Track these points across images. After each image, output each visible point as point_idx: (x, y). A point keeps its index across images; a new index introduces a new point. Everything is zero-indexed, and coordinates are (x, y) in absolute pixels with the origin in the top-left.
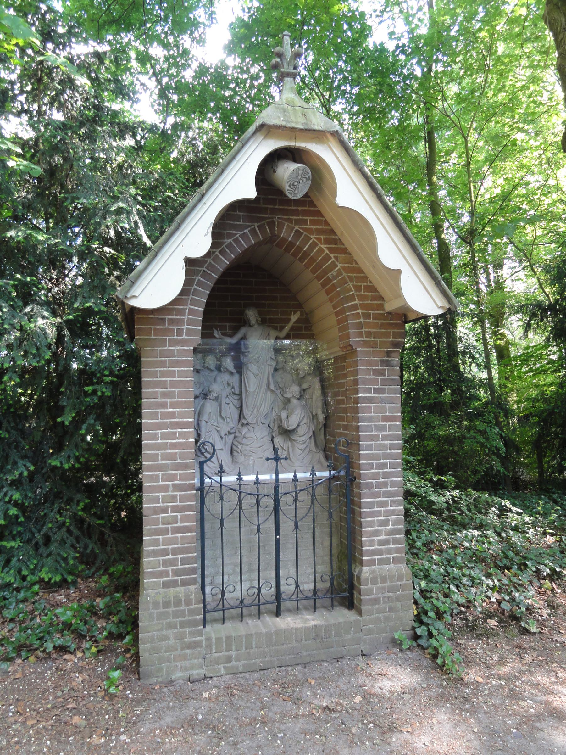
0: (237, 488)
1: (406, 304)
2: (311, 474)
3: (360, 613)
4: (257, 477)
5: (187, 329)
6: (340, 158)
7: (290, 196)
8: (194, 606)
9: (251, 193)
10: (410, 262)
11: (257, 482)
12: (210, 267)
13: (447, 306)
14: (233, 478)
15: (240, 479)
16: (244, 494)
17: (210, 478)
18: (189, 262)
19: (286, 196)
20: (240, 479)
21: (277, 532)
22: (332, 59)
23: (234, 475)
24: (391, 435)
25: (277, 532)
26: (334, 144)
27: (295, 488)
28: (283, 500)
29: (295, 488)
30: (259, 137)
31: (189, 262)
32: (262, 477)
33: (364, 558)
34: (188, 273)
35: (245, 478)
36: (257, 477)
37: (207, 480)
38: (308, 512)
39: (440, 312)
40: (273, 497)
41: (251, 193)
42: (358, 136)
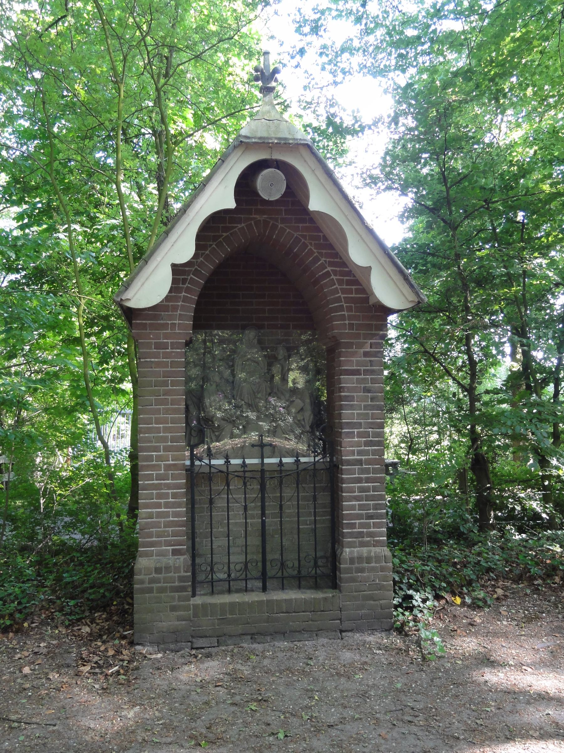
0: (224, 469)
1: (379, 302)
3: (340, 591)
4: (281, 460)
6: (398, 284)
8: (183, 574)
9: (230, 204)
10: (358, 230)
11: (244, 465)
12: (196, 273)
13: (417, 300)
14: (221, 462)
15: (227, 462)
18: (174, 267)
24: (175, 409)
26: (305, 153)
30: (238, 152)
31: (174, 267)
35: (233, 461)
36: (281, 460)
37: (197, 463)
39: (410, 305)
41: (230, 204)
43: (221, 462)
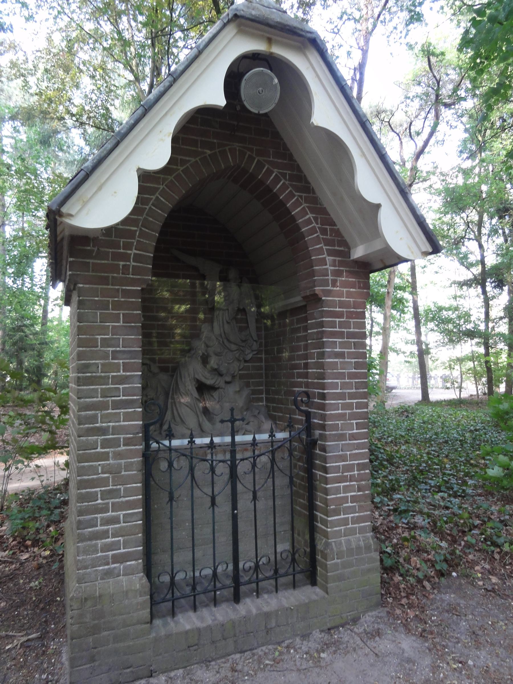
0: (188, 453)
2: (270, 436)
4: (212, 440)
5: (135, 254)
7: (255, 111)
9: (221, 101)
15: (192, 442)
16: (197, 460)
17: (158, 443)
19: (250, 112)
20: (192, 442)
21: (234, 506)
22: (178, 331)
23: (186, 438)
25: (234, 506)
27: (254, 453)
28: (243, 468)
29: (254, 453)
32: (217, 440)
33: (329, 574)
34: (142, 190)
36: (212, 440)
38: (268, 478)
40: (229, 462)
41: (221, 101)
42: (495, 499)
43: (186, 441)
